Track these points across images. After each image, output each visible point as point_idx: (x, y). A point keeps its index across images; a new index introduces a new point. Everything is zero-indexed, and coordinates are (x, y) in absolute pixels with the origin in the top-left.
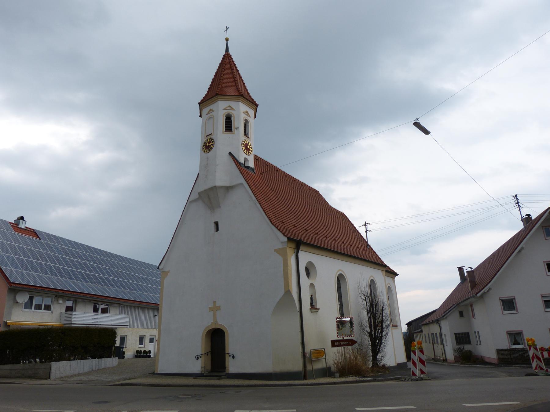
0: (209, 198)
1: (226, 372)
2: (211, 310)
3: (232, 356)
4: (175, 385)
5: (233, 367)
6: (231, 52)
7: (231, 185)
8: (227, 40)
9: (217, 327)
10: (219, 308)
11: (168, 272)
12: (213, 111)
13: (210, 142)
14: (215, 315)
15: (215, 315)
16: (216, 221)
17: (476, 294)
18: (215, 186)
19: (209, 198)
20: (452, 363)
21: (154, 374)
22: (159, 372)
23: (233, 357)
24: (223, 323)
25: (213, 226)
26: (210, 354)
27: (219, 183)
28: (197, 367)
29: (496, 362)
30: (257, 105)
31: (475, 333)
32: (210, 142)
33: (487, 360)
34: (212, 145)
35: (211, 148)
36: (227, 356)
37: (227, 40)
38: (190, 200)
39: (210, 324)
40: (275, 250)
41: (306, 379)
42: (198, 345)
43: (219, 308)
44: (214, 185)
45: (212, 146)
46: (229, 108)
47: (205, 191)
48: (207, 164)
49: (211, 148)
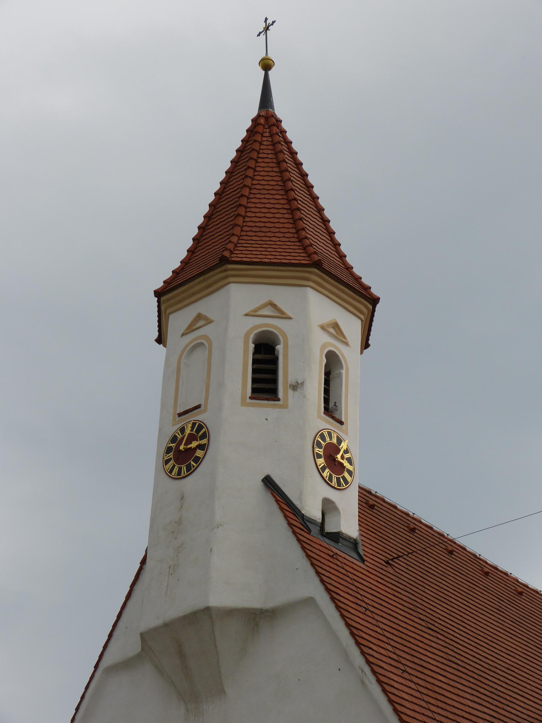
0: (182, 655)
7: (269, 605)
8: (266, 65)
13: (192, 438)
18: (207, 610)
19: (182, 655)
27: (220, 598)
30: (374, 301)
34: (201, 447)
37: (266, 65)
44: (201, 605)
45: (199, 453)
46: (332, 330)
48: (179, 522)
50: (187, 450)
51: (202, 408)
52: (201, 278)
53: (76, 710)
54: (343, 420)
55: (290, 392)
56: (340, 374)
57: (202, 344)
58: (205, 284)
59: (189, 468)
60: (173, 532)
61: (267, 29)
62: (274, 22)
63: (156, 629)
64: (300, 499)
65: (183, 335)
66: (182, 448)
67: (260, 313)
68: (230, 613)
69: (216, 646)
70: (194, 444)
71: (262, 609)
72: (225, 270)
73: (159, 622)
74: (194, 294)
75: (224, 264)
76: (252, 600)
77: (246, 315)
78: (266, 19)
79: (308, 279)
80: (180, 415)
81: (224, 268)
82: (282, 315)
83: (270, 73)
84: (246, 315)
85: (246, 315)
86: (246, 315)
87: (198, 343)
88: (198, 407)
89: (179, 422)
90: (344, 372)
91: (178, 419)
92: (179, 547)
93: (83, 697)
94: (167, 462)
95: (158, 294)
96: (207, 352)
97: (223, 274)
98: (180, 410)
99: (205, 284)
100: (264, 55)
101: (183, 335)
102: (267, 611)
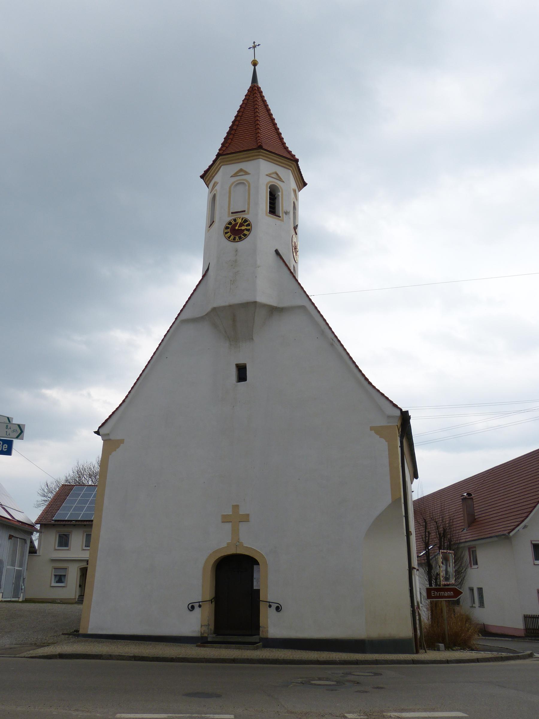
0: (234, 320)
1: (261, 635)
2: (225, 519)
3: (274, 606)
4: (144, 657)
5: (274, 626)
6: (260, 84)
7: (281, 305)
8: (255, 64)
9: (239, 552)
10: (246, 518)
11: (122, 441)
12: (247, 173)
13: (241, 225)
14: (235, 532)
15: (235, 532)
16: (241, 361)
17: (509, 533)
18: (255, 303)
19: (234, 320)
20: (200, 641)
21: (76, 634)
22: (90, 632)
23: (278, 609)
24: (250, 542)
25: (233, 372)
26: (214, 603)
27: (261, 299)
28: (193, 624)
29: (522, 634)
30: (305, 184)
31: (472, 590)
32: (241, 225)
33: (494, 631)
34: (248, 230)
35: (245, 235)
36: (263, 607)
37: (255, 64)
38: (182, 317)
39: (224, 545)
40: (372, 428)
41: (417, 652)
42: (197, 584)
43: (246, 518)
44: (250, 299)
45: (246, 232)
46: (274, 176)
47: (230, 306)
48: (236, 261)
49: (245, 235)
50: (238, 230)
51: (246, 212)
52: (245, 153)
54: (281, 215)
55: (284, 215)
56: (279, 195)
57: (243, 183)
58: (247, 156)
59: (234, 239)
61: (254, 47)
62: (259, 45)
63: (224, 307)
64: (289, 263)
65: (232, 176)
66: (237, 228)
68: (264, 306)
69: (254, 319)
70: (243, 228)
72: (259, 152)
73: (227, 304)
78: (254, 43)
79: (291, 167)
80: (232, 213)
82: (280, 179)
88: (244, 211)
89: (232, 216)
90: (280, 194)
91: (231, 215)
94: (226, 233)
95: (202, 177)
96: (247, 187)
98: (232, 211)
99: (247, 156)
101: (232, 176)
102: (279, 308)
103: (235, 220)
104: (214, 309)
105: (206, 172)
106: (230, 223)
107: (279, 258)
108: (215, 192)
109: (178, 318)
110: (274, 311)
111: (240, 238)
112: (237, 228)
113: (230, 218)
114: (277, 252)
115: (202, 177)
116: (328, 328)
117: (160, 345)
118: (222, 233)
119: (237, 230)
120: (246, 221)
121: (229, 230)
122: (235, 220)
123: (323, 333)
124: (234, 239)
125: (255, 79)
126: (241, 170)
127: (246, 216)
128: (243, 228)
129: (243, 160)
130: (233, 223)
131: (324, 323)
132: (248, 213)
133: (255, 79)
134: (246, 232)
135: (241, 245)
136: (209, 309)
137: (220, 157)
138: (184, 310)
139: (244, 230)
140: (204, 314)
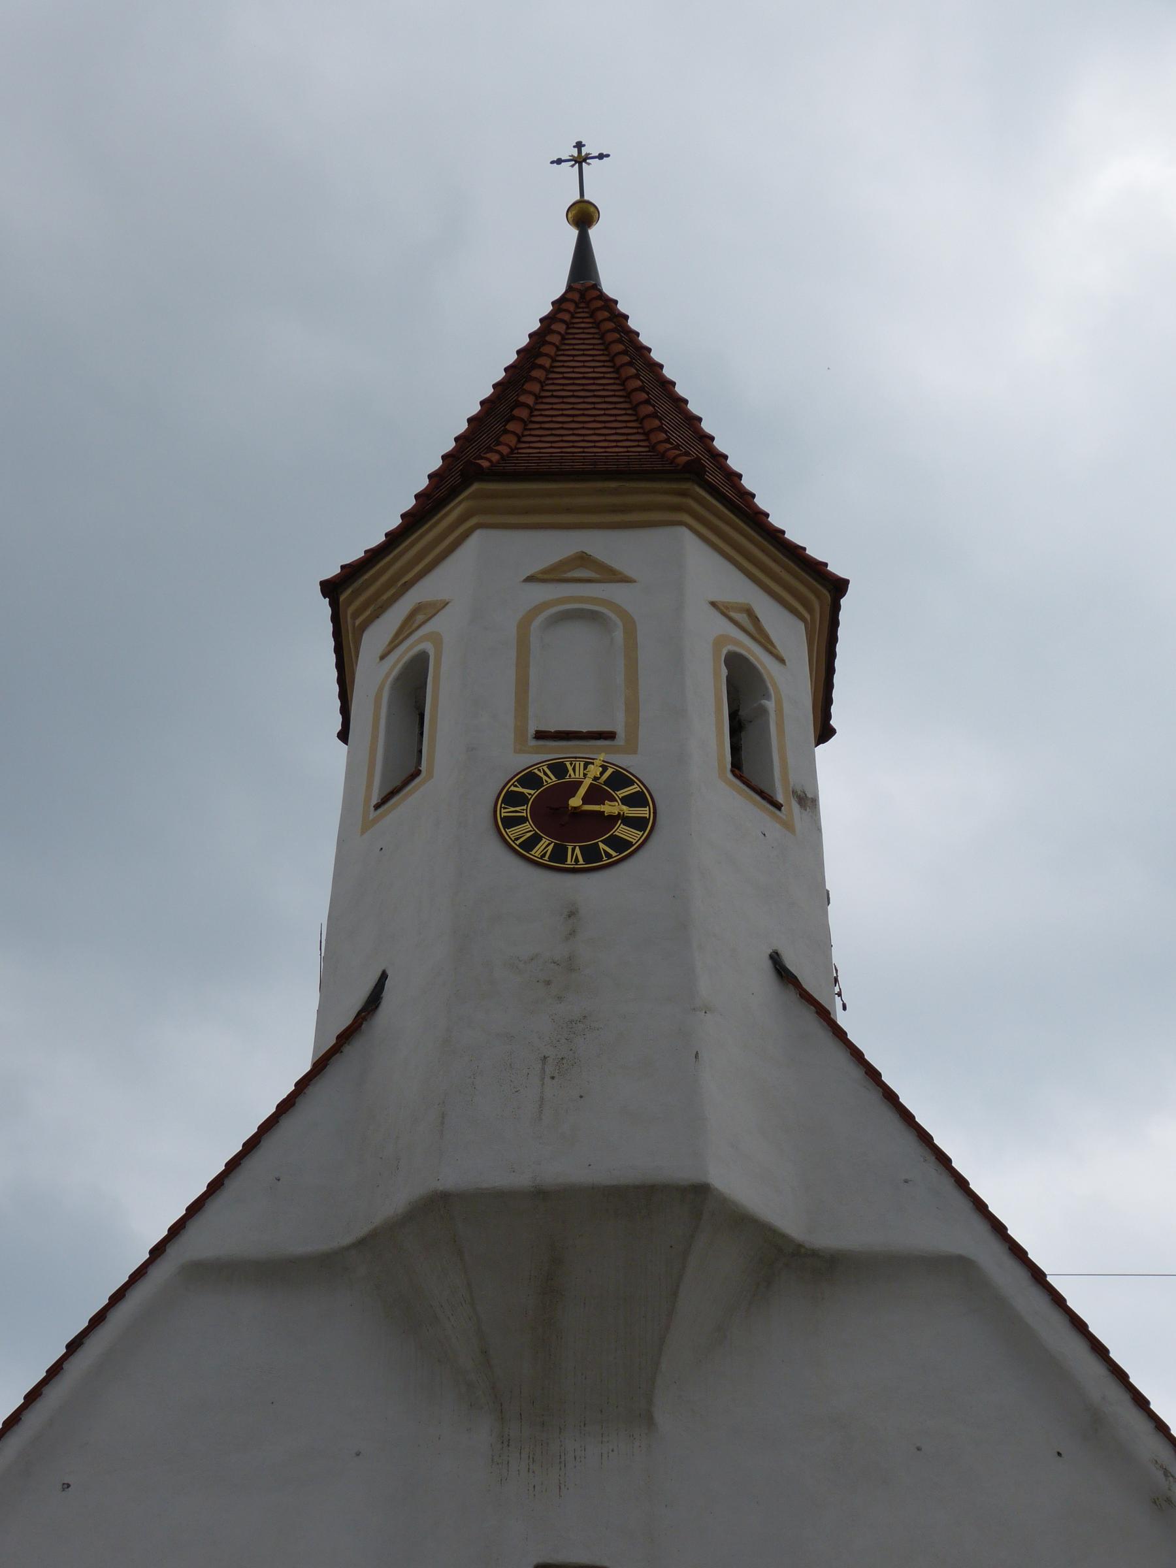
7: (824, 1239)
8: (583, 216)
12: (611, 575)
13: (596, 794)
18: (700, 1192)
34: (638, 824)
35: (620, 845)
38: (200, 1244)
46: (742, 618)
47: (541, 1195)
48: (570, 965)
50: (577, 813)
51: (620, 741)
53: (68, 1346)
56: (764, 711)
59: (559, 854)
60: (548, 983)
61: (580, 160)
63: (502, 1198)
65: (530, 579)
66: (575, 802)
67: (732, 614)
68: (742, 1222)
71: (800, 1246)
72: (684, 494)
73: (522, 1180)
74: (569, 510)
75: (687, 480)
76: (787, 1215)
77: (713, 604)
78: (579, 145)
79: (810, 610)
80: (540, 735)
81: (685, 486)
83: (593, 233)
84: (713, 604)
85: (713, 604)
86: (713, 604)
87: (582, 610)
88: (610, 736)
92: (571, 1022)
93: (98, 1320)
95: (330, 588)
96: (619, 635)
97: (677, 500)
100: (578, 197)
101: (530, 579)
102: (814, 1254)
103: (559, 769)
104: (437, 1207)
105: (351, 572)
106: (530, 779)
107: (792, 995)
108: (428, 647)
109: (172, 1250)
110: (785, 1266)
111: (592, 854)
112: (575, 802)
113: (536, 758)
114: (776, 959)
115: (330, 588)
116: (1126, 1398)
117: (32, 1396)
118: (485, 811)
119: (572, 816)
120: (620, 779)
121: (524, 811)
122: (559, 769)
123: (1093, 1427)
124: (559, 854)
125: (583, 261)
126: (583, 559)
127: (624, 761)
128: (608, 808)
129: (594, 519)
130: (550, 780)
131: (1100, 1369)
132: (632, 747)
133: (583, 261)
134: (622, 831)
135: (591, 889)
136: (396, 1198)
137: (476, 486)
138: (213, 1206)
139: (613, 819)
140: (347, 1240)
